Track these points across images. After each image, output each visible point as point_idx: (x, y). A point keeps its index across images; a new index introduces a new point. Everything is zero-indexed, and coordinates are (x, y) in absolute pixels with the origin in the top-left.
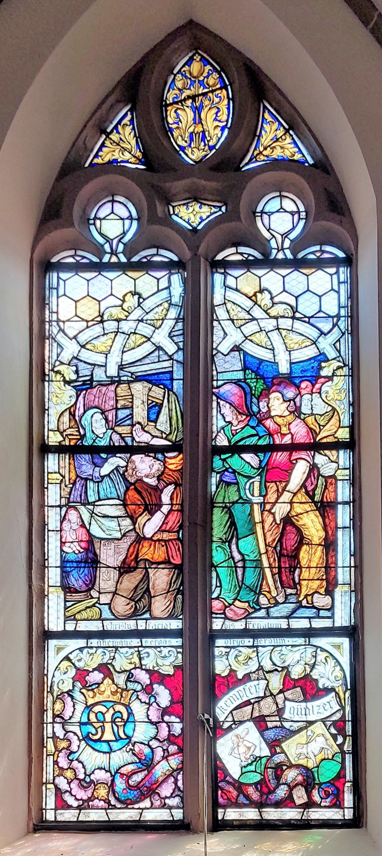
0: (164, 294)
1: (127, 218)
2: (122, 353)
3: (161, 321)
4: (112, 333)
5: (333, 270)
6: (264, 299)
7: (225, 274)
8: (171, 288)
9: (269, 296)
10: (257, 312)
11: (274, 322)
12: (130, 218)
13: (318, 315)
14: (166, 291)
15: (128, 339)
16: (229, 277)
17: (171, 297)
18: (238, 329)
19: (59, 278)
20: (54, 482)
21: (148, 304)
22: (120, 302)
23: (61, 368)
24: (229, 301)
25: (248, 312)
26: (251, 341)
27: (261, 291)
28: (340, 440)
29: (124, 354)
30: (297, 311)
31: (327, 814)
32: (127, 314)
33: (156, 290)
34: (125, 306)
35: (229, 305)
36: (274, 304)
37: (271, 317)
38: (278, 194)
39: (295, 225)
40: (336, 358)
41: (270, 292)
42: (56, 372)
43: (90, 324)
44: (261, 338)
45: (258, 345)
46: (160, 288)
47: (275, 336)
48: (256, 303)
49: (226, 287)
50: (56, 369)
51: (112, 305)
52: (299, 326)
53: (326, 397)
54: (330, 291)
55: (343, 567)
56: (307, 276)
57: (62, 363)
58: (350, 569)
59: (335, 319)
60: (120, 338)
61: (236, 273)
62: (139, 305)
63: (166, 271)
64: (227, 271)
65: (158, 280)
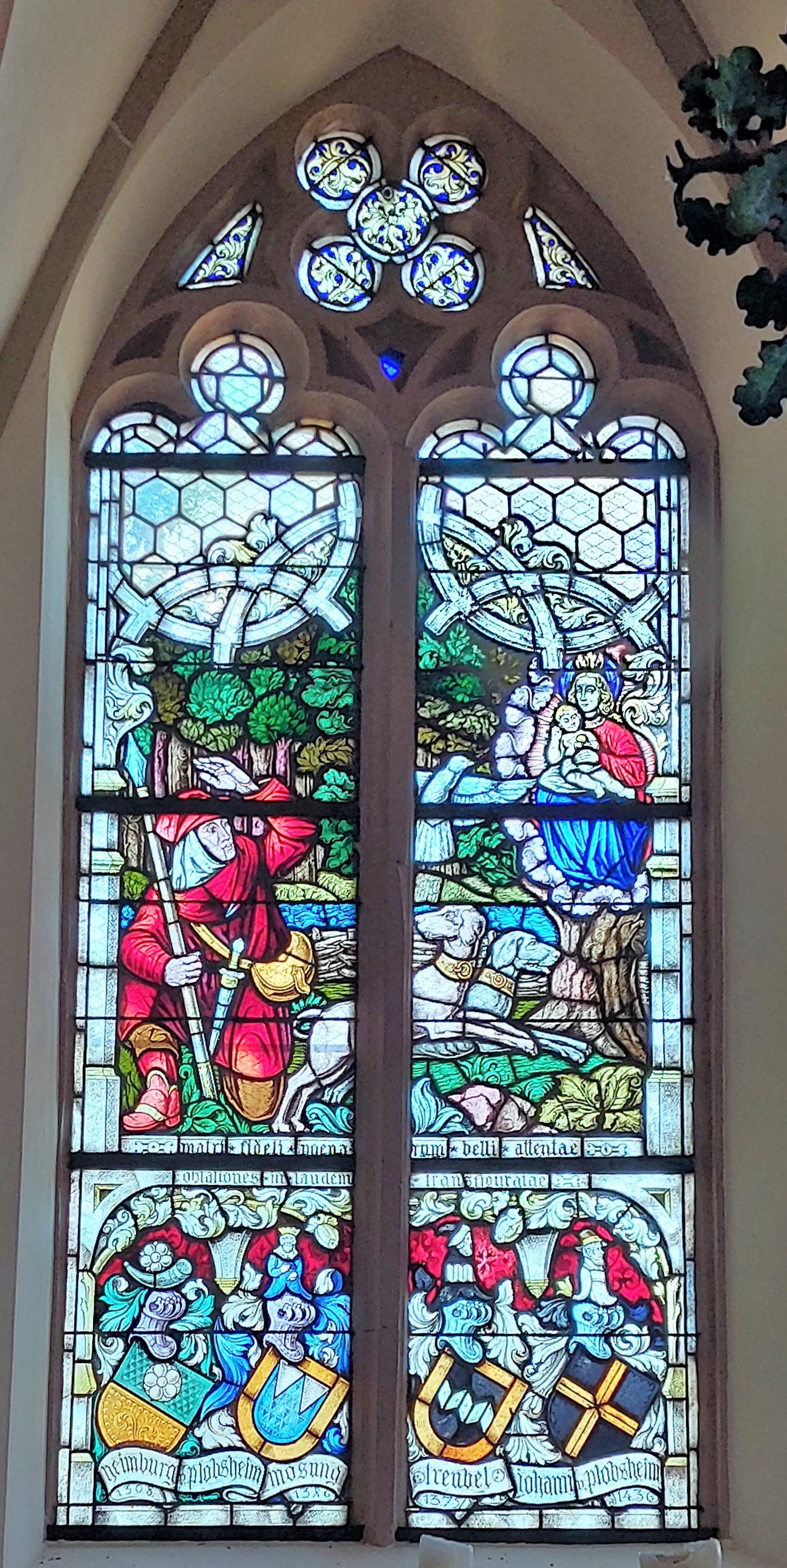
0: (325, 519)
5: (647, 484)
8: (340, 508)
10: (507, 560)
11: (534, 579)
13: (235, 372)
19: (122, 482)
20: (104, 870)
21: (292, 538)
28: (656, 801)
32: (254, 554)
33: (310, 510)
37: (529, 570)
38: (540, 340)
44: (511, 607)
46: (319, 505)
47: (538, 607)
50: (113, 654)
52: (583, 586)
53: (632, 719)
60: (241, 599)
63: (329, 475)
64: (447, 480)
65: (314, 491)
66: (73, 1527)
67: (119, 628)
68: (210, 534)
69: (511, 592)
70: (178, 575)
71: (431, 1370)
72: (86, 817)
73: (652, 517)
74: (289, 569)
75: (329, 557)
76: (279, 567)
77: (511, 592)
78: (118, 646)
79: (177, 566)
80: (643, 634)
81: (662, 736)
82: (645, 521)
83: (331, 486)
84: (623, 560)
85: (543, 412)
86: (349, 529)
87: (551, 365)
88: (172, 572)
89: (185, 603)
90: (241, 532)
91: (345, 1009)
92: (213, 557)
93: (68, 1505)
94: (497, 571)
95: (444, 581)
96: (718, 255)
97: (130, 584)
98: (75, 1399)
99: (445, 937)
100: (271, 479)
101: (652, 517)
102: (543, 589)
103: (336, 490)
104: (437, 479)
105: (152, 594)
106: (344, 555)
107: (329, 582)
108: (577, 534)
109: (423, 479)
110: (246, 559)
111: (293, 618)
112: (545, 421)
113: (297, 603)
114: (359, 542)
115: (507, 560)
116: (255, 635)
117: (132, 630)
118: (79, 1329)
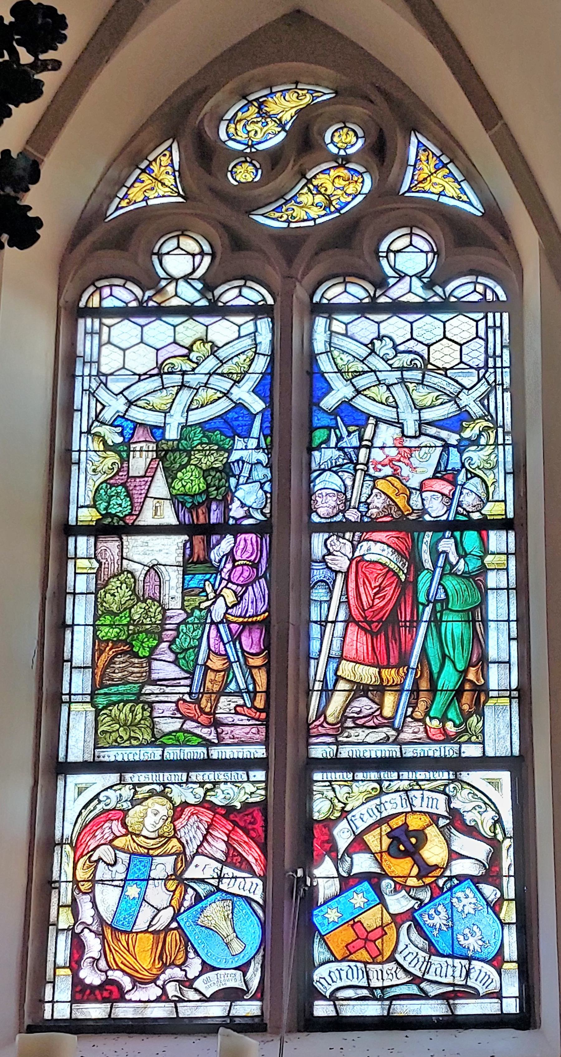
1: (199, 254)
2: (187, 412)
4: (174, 387)
6: (385, 348)
7: (330, 318)
9: (391, 344)
11: (398, 374)
12: (202, 253)
15: (195, 395)
16: (334, 322)
21: (222, 354)
23: (104, 430)
24: (335, 348)
26: (365, 396)
27: (380, 338)
29: (190, 413)
31: (412, 1007)
32: (195, 365)
34: (193, 356)
36: (397, 353)
39: (196, 265)
41: (391, 339)
42: (95, 434)
43: (142, 377)
44: (381, 393)
45: (375, 400)
47: (398, 391)
50: (92, 432)
53: (469, 464)
54: (242, 325)
57: (103, 423)
58: (507, 690)
59: (483, 371)
60: (185, 395)
61: (346, 318)
62: (213, 353)
66: (57, 1020)
68: (163, 355)
69: (380, 383)
70: (139, 380)
73: (482, 333)
75: (250, 366)
77: (380, 383)
78: (97, 426)
80: (476, 410)
82: (477, 336)
83: (252, 323)
85: (406, 275)
86: (265, 347)
87: (411, 244)
90: (185, 351)
91: (316, 816)
93: (53, 1002)
94: (372, 371)
96: (13, 112)
98: (61, 909)
99: (488, 904)
101: (482, 333)
102: (402, 381)
103: (256, 325)
106: (260, 364)
107: (250, 382)
108: (429, 346)
110: (189, 369)
111: (223, 405)
112: (408, 279)
113: (225, 395)
116: (196, 417)
117: (107, 415)
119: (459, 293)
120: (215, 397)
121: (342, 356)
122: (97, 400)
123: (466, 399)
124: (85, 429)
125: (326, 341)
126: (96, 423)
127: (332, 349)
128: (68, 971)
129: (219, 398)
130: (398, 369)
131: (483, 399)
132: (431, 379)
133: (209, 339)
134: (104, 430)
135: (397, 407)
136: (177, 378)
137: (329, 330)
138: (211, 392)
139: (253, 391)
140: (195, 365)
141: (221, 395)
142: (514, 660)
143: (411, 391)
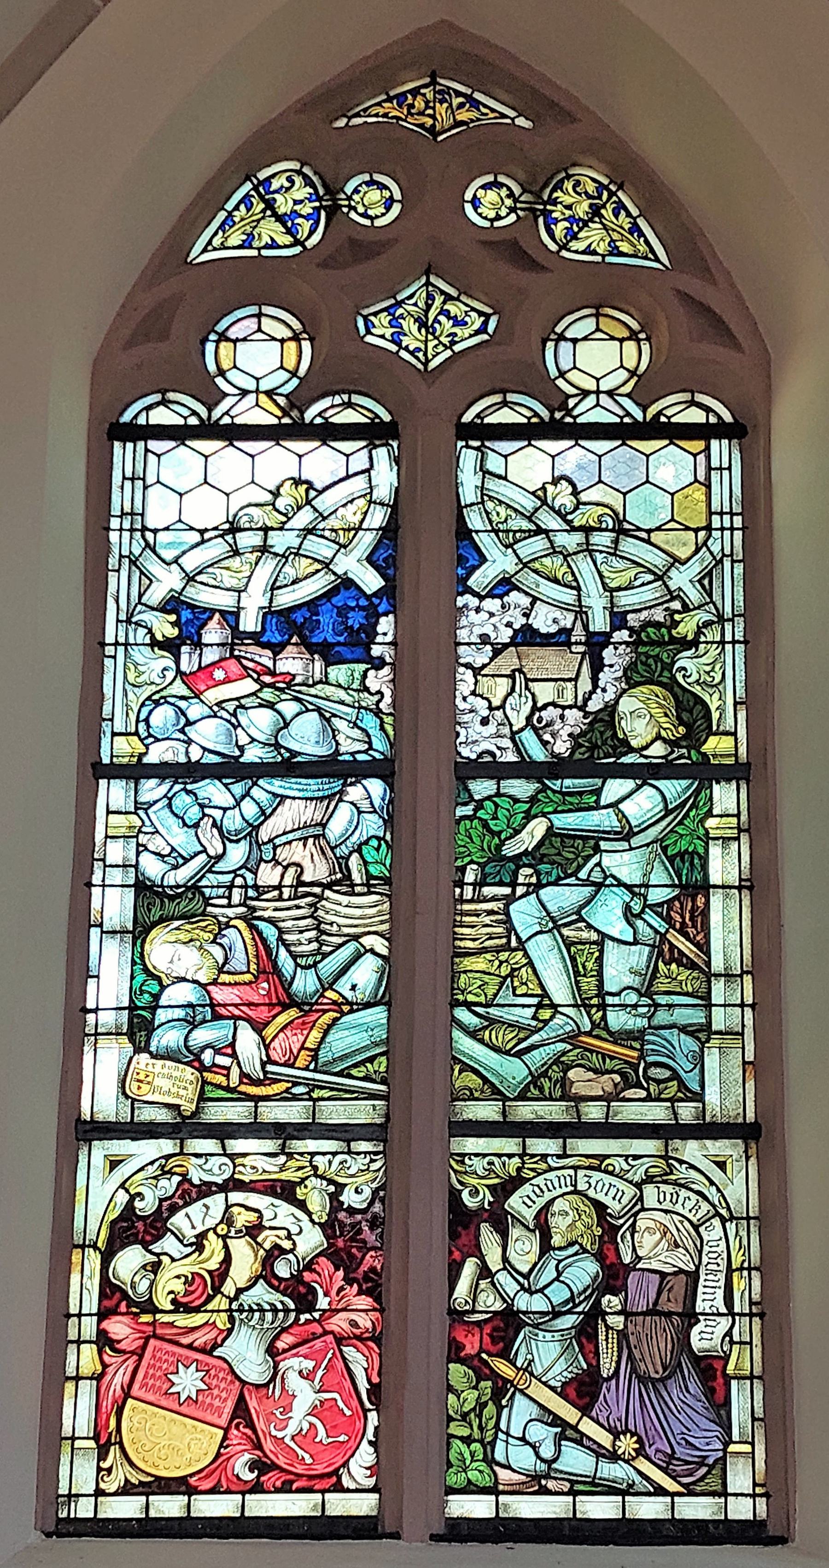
0: (358, 484)
3: (353, 532)
5: (699, 445)
8: (372, 472)
10: (550, 521)
11: (579, 537)
14: (362, 476)
17: (371, 487)
18: (174, 566)
19: (147, 450)
22: (269, 497)
23: (148, 617)
25: (530, 519)
27: (555, 482)
30: (625, 520)
32: (284, 519)
33: (344, 474)
34: (281, 503)
35: (490, 505)
37: (574, 529)
40: (703, 605)
42: (136, 623)
46: (350, 473)
48: (544, 502)
49: (486, 472)
50: (134, 620)
51: (245, 504)
55: (724, 1006)
56: (252, 456)
59: (702, 534)
60: (268, 566)
61: (505, 446)
67: (140, 596)
69: (554, 551)
70: (203, 542)
71: (721, 816)
72: (103, 783)
73: (701, 477)
74: (319, 533)
76: (309, 531)
77: (554, 551)
78: (140, 613)
79: (202, 532)
80: (694, 595)
81: (716, 696)
82: (696, 480)
84: (672, 520)
87: (598, 329)
88: (196, 537)
89: (210, 570)
92: (244, 522)
95: (485, 542)
97: (154, 551)
100: (301, 446)
103: (370, 452)
104: (476, 444)
105: (176, 561)
106: (378, 518)
109: (460, 444)
114: (395, 508)
115: (550, 521)
116: (285, 599)
117: (156, 595)
118: (83, 1312)
119: (669, 412)
120: (311, 569)
121: (498, 508)
122: (142, 573)
123: (680, 579)
124: (123, 617)
125: (477, 487)
126: (139, 607)
127: (486, 498)
128: (92, 1444)
129: (318, 571)
130: (581, 529)
131: (703, 578)
132: (628, 546)
133: (303, 478)
134: (148, 617)
135: (578, 589)
136: (256, 539)
137: (481, 469)
138: (305, 562)
139: (369, 559)
140: (284, 519)
141: (319, 567)
142: (756, 1340)
143: (599, 563)
